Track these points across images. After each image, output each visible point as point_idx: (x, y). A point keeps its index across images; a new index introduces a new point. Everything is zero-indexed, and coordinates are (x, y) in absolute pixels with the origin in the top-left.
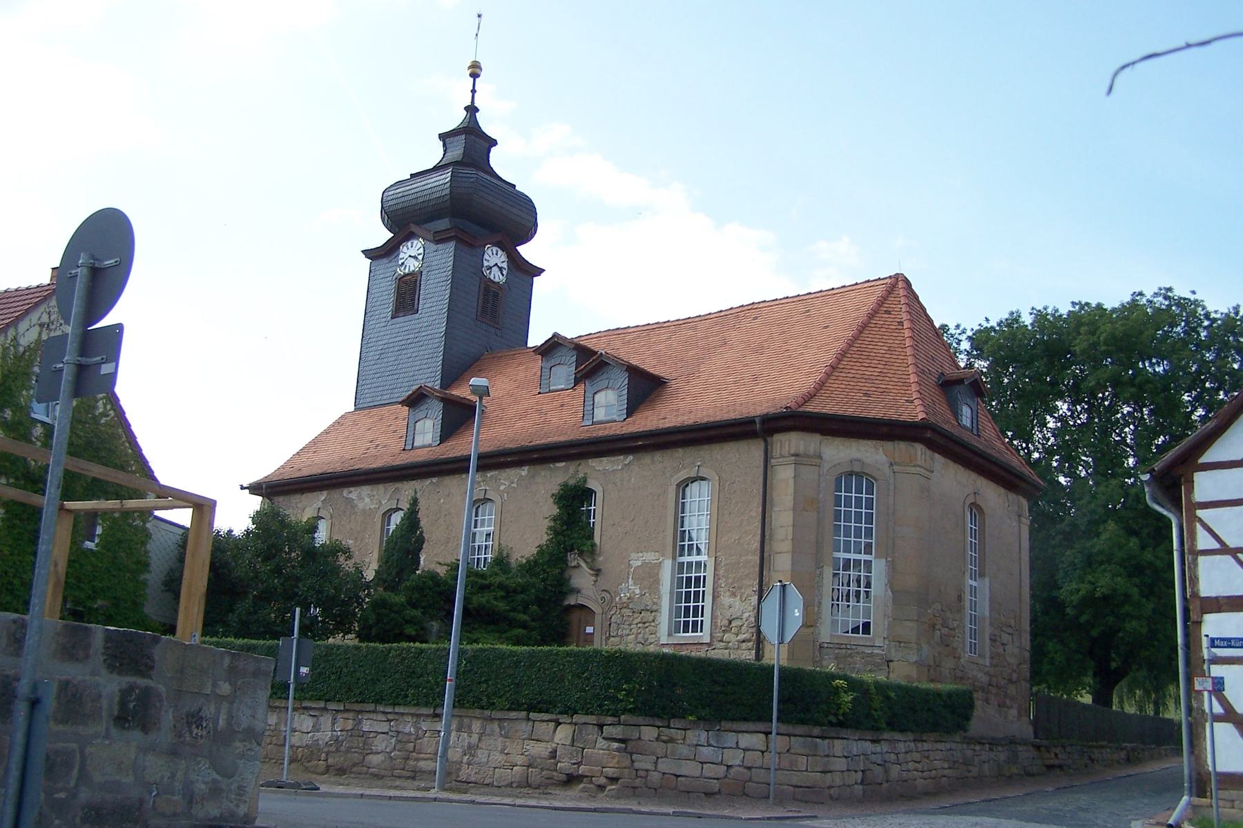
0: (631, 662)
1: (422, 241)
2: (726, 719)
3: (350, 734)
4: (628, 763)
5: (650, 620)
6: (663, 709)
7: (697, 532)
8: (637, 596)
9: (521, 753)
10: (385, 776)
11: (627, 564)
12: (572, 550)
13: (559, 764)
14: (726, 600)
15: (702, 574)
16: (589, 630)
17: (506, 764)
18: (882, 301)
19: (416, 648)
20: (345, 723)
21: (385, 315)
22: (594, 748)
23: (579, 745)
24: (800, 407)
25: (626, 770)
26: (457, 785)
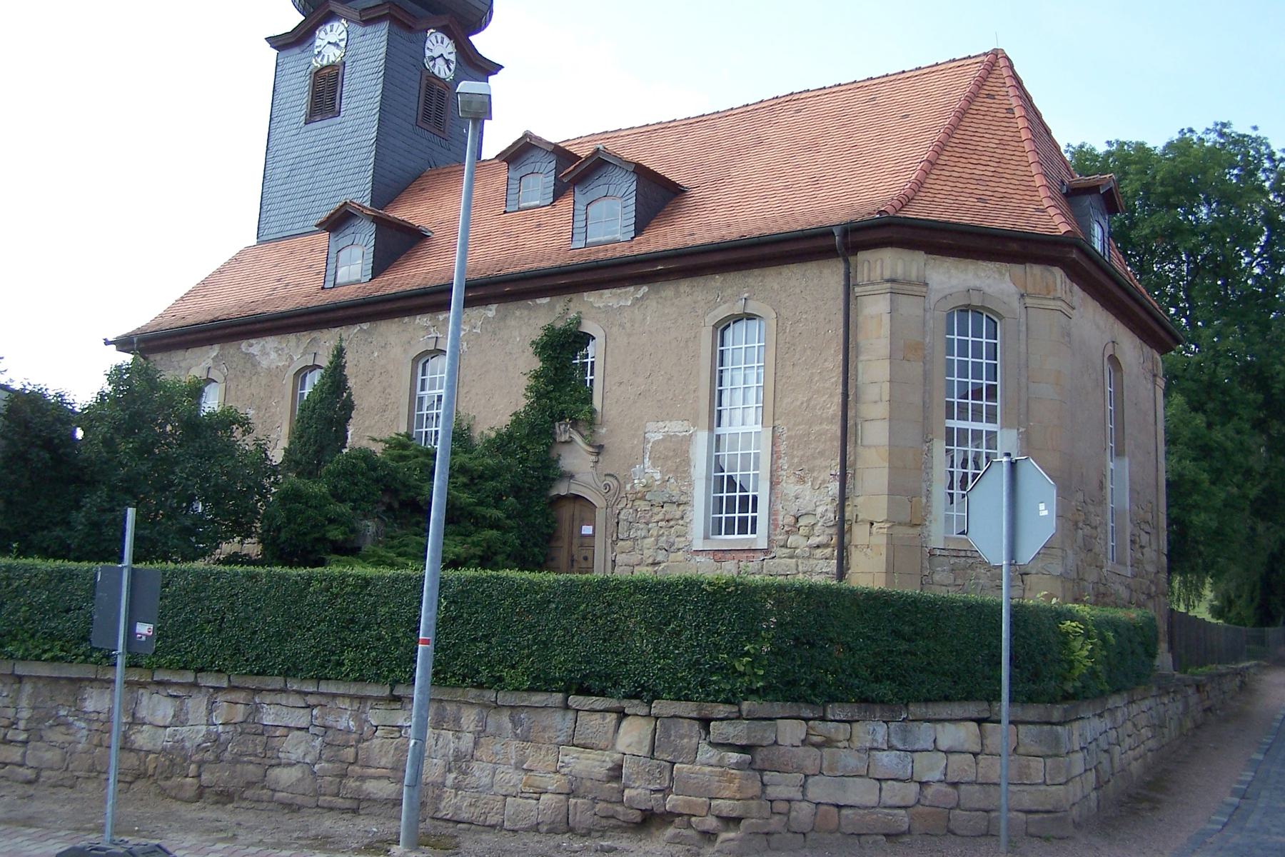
0: (757, 601)
1: (345, 22)
2: (917, 700)
3: (239, 730)
4: (755, 789)
5: (677, 517)
6: (813, 686)
7: (731, 392)
8: (658, 483)
9: (553, 769)
10: (304, 807)
11: (642, 438)
12: (562, 418)
13: (627, 791)
14: (790, 487)
16: (587, 530)
17: (527, 789)
18: (981, 82)
19: (357, 577)
20: (230, 710)
21: (296, 120)
22: (693, 762)
23: (665, 756)
24: (897, 212)
25: (754, 803)
26: (435, 827)
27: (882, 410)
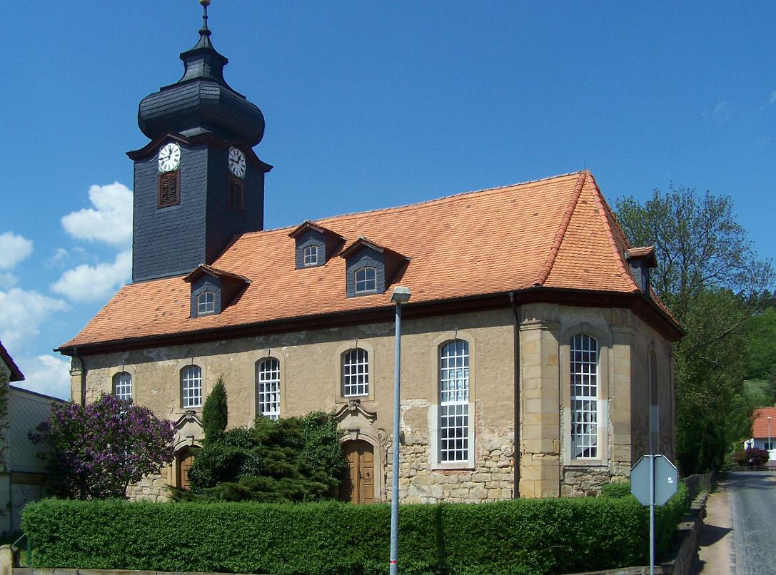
14: (486, 435)
15: (463, 415)
27: (537, 393)
